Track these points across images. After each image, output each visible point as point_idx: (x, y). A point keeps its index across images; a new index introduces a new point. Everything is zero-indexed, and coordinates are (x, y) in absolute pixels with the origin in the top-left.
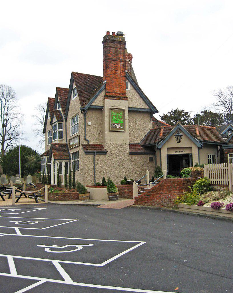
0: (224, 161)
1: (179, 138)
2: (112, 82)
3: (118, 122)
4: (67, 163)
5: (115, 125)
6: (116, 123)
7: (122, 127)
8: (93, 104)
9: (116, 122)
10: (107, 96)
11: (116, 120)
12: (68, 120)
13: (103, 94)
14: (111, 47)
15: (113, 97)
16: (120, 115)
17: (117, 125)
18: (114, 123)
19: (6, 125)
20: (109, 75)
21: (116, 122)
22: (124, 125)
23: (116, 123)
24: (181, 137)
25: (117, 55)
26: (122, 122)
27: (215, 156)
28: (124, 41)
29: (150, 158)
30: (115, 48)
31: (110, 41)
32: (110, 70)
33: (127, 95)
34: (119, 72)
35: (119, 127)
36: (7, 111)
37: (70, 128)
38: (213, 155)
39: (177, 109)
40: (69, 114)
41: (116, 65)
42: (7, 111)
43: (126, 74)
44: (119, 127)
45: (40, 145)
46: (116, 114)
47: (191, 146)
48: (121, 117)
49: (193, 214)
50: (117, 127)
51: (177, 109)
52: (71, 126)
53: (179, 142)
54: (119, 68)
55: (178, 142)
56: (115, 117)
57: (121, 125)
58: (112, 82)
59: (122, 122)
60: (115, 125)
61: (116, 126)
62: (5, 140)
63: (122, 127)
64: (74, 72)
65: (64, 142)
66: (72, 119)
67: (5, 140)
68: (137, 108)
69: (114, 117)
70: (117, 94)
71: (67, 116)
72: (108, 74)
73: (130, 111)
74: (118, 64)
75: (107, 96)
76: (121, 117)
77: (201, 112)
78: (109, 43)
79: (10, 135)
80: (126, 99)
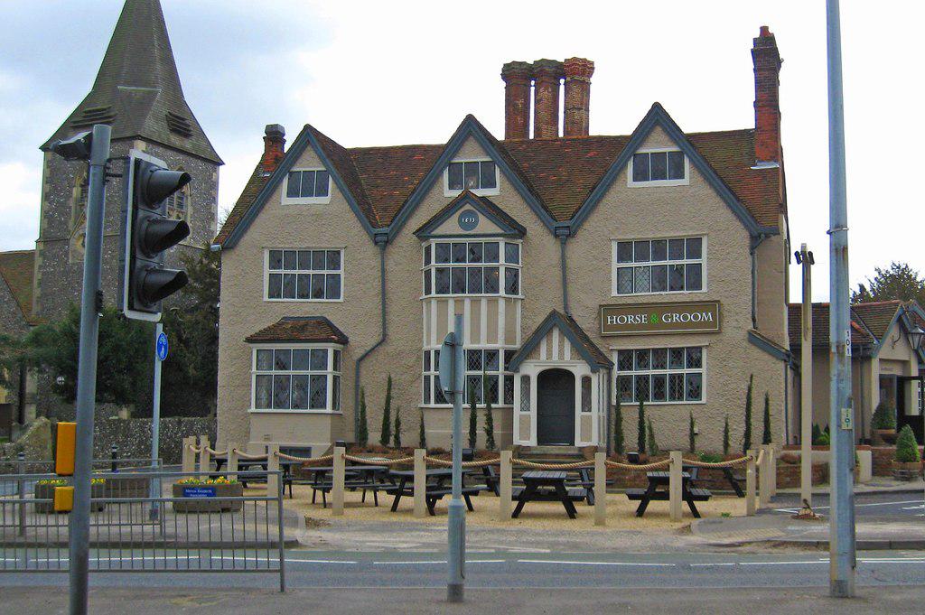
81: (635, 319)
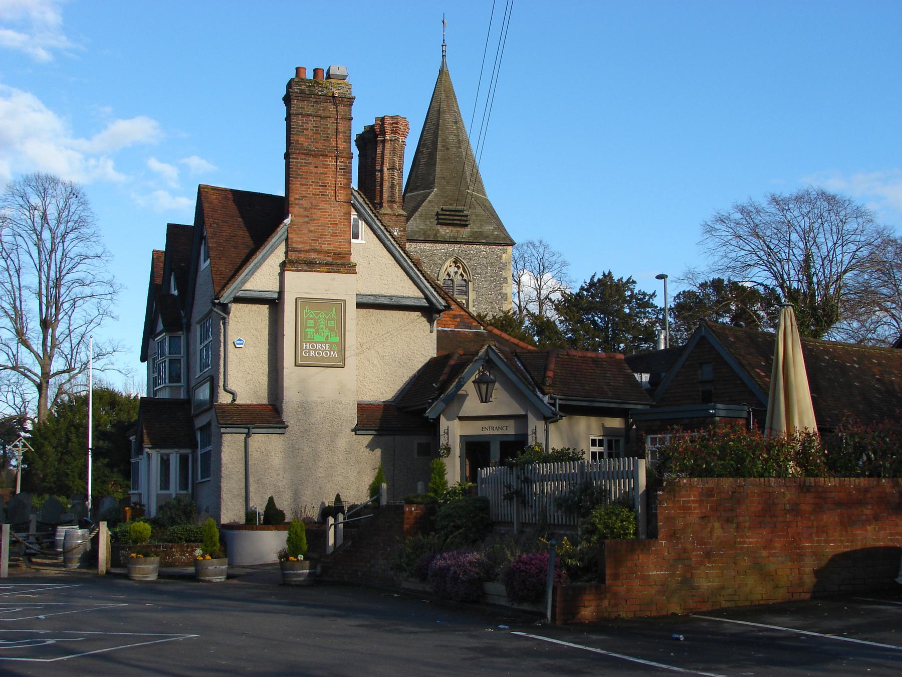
0: (618, 456)
1: (484, 387)
2: (306, 219)
3: (323, 339)
4: (184, 460)
5: (313, 346)
6: (316, 343)
7: (335, 354)
8: (248, 286)
9: (318, 338)
10: (292, 262)
11: (317, 332)
12: (193, 328)
13: (279, 255)
14: (308, 115)
15: (310, 266)
16: (330, 319)
17: (319, 346)
18: (310, 342)
19: (57, 320)
20: (299, 199)
21: (318, 338)
22: (342, 348)
23: (316, 343)
24: (490, 386)
25: (327, 139)
26: (337, 339)
27: (617, 441)
28: (348, 95)
29: (419, 445)
30: (319, 119)
31: (304, 96)
32: (301, 184)
33: (353, 259)
34: (330, 192)
35: (326, 354)
36: (60, 273)
37: (195, 353)
38: (609, 438)
39: (608, 276)
40: (194, 310)
41: (321, 170)
42: (60, 273)
43: (352, 194)
44: (326, 354)
45: (828, 259)
46: (317, 314)
47: (523, 413)
48: (331, 324)
49: (48, 559)
50: (319, 354)
51: (608, 276)
52: (199, 347)
53: (485, 399)
54: (330, 180)
55: (482, 402)
56: (315, 324)
57: (331, 347)
58: (306, 219)
59: (337, 339)
60: (313, 346)
61: (315, 350)
62: (52, 373)
63: (335, 354)
64: (206, 187)
65: (182, 396)
66: (201, 326)
67: (52, 373)
68: (385, 296)
69: (310, 323)
70: (322, 256)
71: (191, 316)
72: (297, 196)
73: (360, 305)
74: (329, 165)
75: (292, 262)
76: (331, 324)
77: (702, 285)
78: (300, 104)
79: (69, 357)
80: (350, 268)
81: (321, 347)
